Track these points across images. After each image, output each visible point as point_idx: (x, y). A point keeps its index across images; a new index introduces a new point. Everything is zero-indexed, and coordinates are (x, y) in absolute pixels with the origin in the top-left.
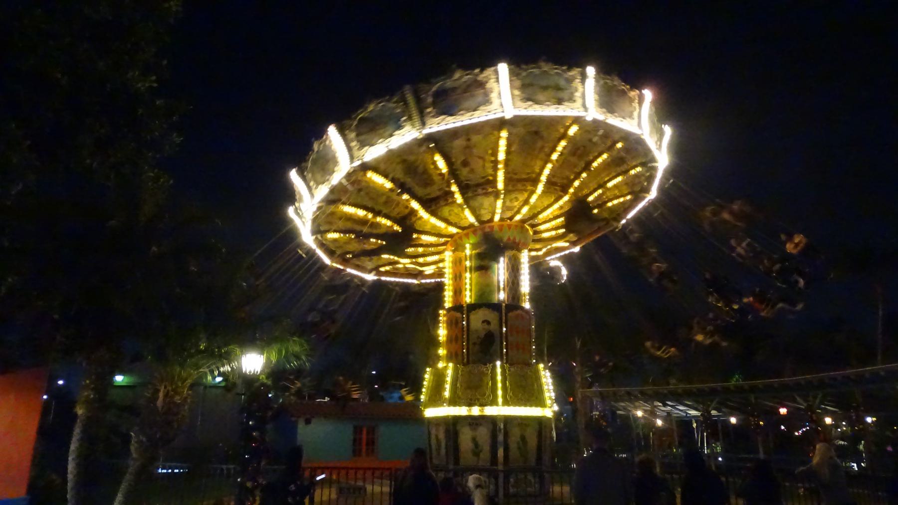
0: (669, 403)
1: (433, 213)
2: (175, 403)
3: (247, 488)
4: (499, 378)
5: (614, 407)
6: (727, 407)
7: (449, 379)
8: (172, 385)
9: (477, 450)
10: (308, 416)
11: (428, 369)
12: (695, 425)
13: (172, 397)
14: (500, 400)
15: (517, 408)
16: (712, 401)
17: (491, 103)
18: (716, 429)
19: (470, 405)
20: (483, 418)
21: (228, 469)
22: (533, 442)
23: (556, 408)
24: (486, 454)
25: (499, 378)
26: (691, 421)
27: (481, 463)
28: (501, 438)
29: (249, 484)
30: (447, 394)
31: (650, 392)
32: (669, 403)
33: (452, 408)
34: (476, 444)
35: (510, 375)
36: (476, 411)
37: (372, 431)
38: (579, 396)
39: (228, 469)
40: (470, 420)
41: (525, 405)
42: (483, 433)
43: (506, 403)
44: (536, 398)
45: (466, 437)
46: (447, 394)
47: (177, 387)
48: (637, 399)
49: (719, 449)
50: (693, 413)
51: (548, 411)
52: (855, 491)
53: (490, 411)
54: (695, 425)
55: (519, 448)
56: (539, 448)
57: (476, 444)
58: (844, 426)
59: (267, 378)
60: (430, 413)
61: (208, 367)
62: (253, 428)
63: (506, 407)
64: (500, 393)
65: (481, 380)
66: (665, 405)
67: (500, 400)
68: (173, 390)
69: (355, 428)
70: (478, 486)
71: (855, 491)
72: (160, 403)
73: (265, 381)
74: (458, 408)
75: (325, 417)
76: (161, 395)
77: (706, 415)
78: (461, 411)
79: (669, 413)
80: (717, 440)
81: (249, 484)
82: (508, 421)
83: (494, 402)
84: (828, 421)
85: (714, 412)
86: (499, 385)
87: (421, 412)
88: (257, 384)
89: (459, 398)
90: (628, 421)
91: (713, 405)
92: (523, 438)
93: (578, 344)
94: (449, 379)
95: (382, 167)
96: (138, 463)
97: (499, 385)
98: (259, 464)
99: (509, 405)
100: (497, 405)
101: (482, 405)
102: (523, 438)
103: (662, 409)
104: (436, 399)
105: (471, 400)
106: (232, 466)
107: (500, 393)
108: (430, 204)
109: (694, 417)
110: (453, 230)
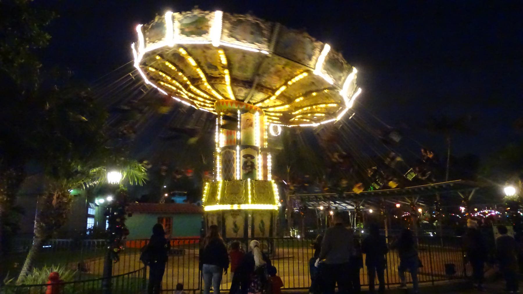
0: (338, 202)
1: (212, 86)
2: (63, 203)
3: (114, 252)
4: (249, 188)
5: (307, 204)
6: (368, 204)
7: (220, 189)
8: (61, 191)
9: (236, 228)
10: (130, 212)
11: (207, 183)
12: (350, 214)
13: (62, 199)
14: (250, 201)
15: (259, 205)
16: (361, 201)
17: (206, 32)
18: (361, 216)
19: (232, 203)
20: (239, 211)
21: (98, 242)
22: (267, 223)
23: (280, 205)
24: (241, 232)
25: (249, 188)
26: (348, 212)
27: (238, 237)
28: (250, 223)
29: (115, 250)
30: (219, 197)
31: (328, 196)
32: (338, 202)
33: (221, 205)
34: (235, 226)
35: (255, 186)
36: (235, 207)
37: (169, 220)
38: (288, 199)
39: (98, 242)
40: (232, 212)
41: (264, 203)
42: (240, 220)
43: (253, 202)
44: (270, 200)
45: (229, 223)
46: (219, 197)
47: (64, 192)
48: (320, 200)
49: (362, 226)
50: (350, 207)
51: (276, 206)
52: (437, 246)
53: (243, 207)
54: (350, 214)
55: (260, 228)
56: (271, 226)
57: (235, 226)
58: (427, 214)
59: (124, 186)
60: (208, 208)
61: (83, 181)
62: (116, 217)
63: (253, 205)
64: (250, 196)
65: (239, 189)
66: (335, 203)
67: (250, 201)
68: (62, 194)
69: (158, 218)
70: (256, 246)
71: (437, 246)
72: (54, 202)
73: (123, 188)
74: (225, 205)
75: (141, 213)
76: (55, 197)
77: (358, 210)
78: (227, 207)
79: (336, 208)
80: (362, 221)
81: (115, 250)
82: (254, 212)
83: (246, 202)
84: (420, 210)
85: (361, 207)
86: (250, 192)
87: (202, 208)
88: (119, 190)
89: (226, 199)
90: (314, 212)
91: (361, 203)
92: (262, 222)
93: (289, 170)
94: (220, 189)
95: (189, 50)
96: (39, 240)
97: (250, 192)
98: (121, 238)
99: (254, 203)
100: (248, 203)
101: (239, 204)
102: (262, 222)
103: (333, 205)
104: (212, 199)
105: (233, 201)
106: (249, 206)
107: (250, 196)
108: (211, 79)
109: (350, 209)
110: (220, 97)
